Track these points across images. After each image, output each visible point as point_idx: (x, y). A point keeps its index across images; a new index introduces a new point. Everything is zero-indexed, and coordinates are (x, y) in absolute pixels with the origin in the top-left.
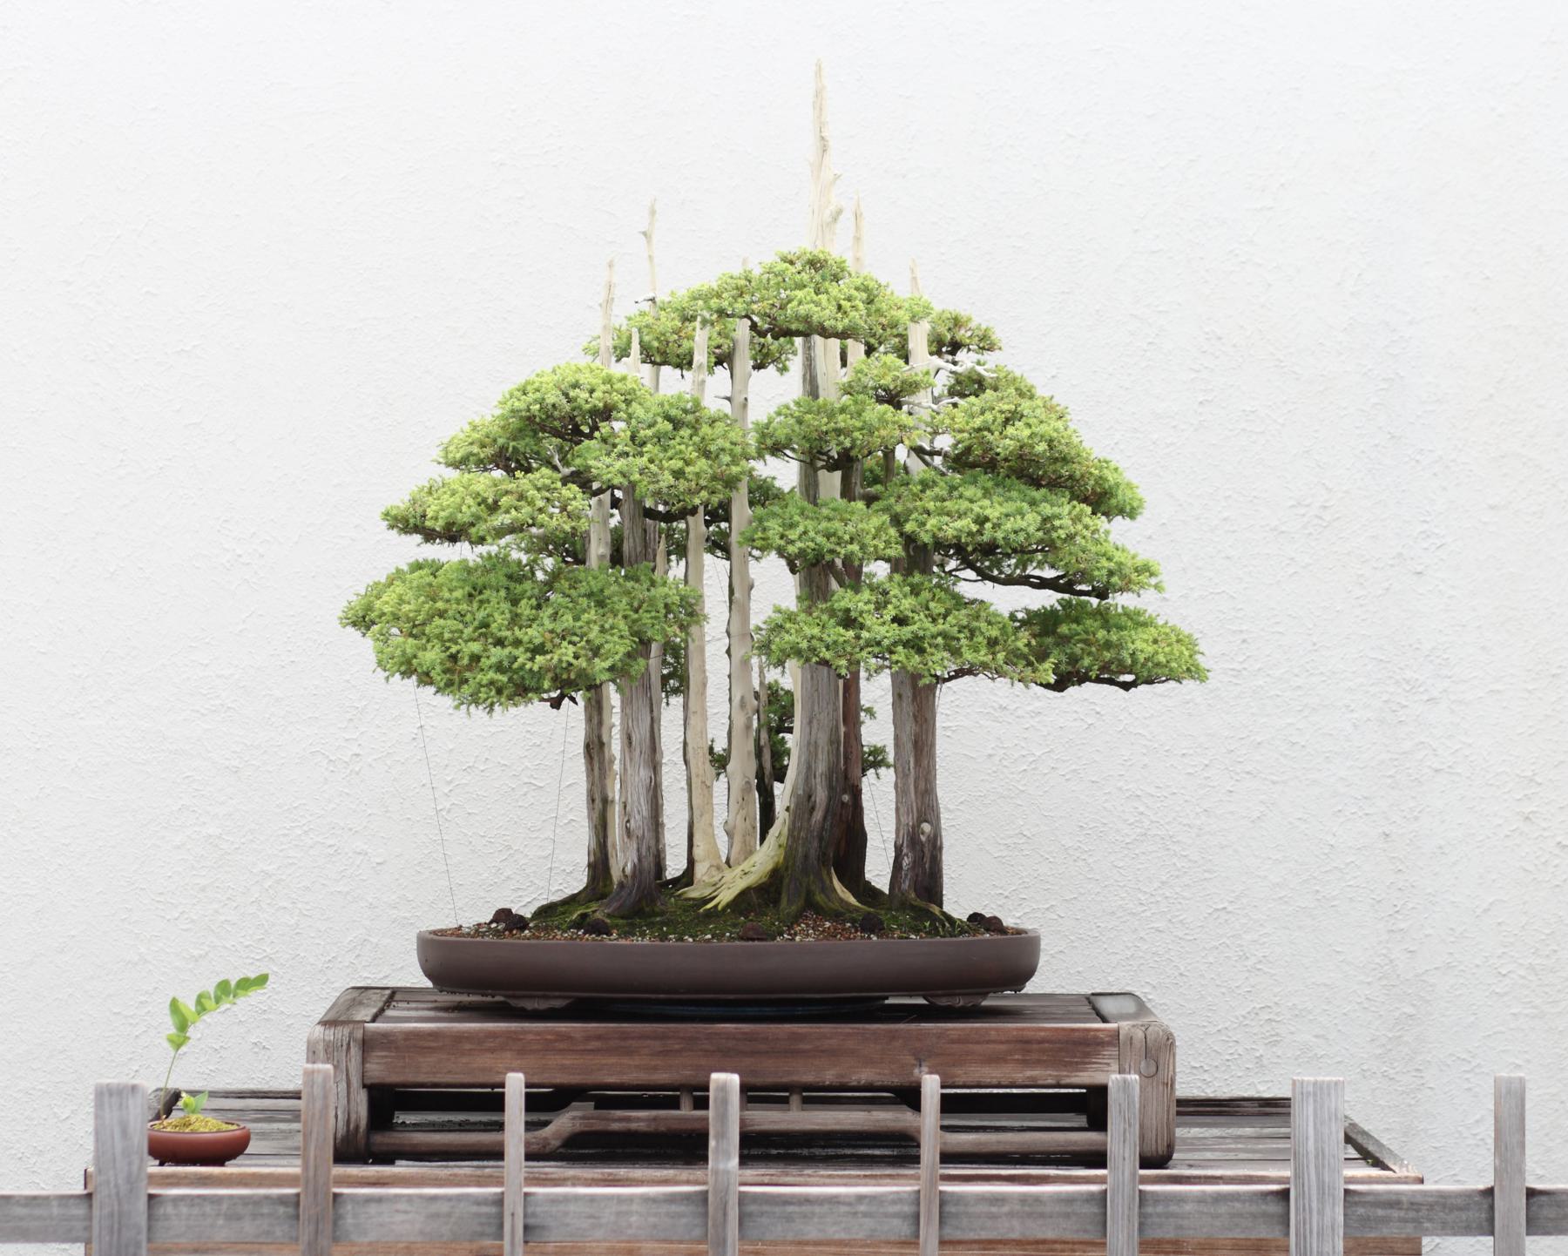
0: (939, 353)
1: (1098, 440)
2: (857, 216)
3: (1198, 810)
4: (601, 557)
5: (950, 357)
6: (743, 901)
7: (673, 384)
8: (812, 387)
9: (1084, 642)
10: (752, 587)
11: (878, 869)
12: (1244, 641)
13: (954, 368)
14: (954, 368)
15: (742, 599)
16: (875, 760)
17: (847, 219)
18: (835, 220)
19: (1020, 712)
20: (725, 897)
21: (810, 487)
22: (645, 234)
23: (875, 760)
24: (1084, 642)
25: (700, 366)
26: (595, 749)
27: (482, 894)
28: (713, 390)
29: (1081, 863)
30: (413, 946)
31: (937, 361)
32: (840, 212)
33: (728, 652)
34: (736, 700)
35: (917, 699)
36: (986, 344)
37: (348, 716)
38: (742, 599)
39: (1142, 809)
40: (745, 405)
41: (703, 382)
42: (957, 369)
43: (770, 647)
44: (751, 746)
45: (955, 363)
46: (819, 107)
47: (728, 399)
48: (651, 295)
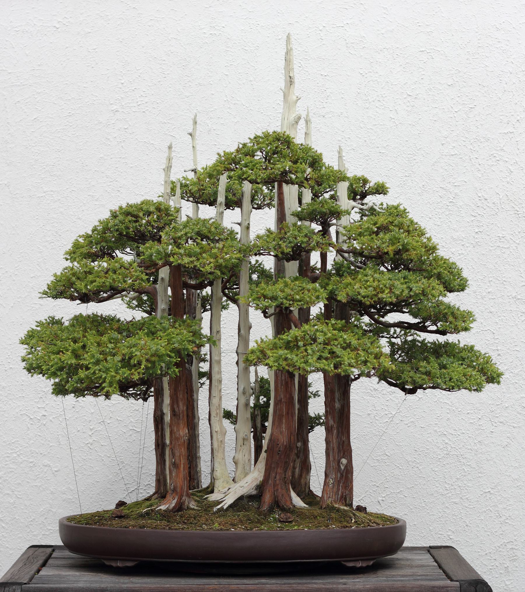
0: (354, 199)
1: (449, 246)
2: (307, 122)
3: (476, 441)
4: (163, 310)
5: (360, 202)
6: (239, 504)
7: (207, 212)
8: (281, 217)
9: (438, 361)
10: (250, 327)
11: (317, 482)
12: (499, 355)
13: (362, 207)
14: (362, 207)
15: (234, 336)
16: (314, 422)
17: (302, 122)
18: (297, 123)
19: (384, 392)
20: (229, 501)
21: (280, 270)
22: (191, 135)
23: (314, 422)
24: (438, 361)
25: (221, 204)
26: (158, 420)
27: (109, 486)
28: (231, 218)
29: (416, 469)
30: (56, 527)
31: (352, 203)
32: (299, 118)
33: (237, 363)
34: (241, 389)
35: (339, 388)
36: (380, 190)
37: (40, 396)
38: (234, 336)
39: (447, 441)
40: (248, 228)
41: (223, 212)
42: (365, 207)
43: (261, 356)
44: (249, 416)
45: (363, 204)
46: (288, 61)
47: (239, 224)
48: (194, 168)
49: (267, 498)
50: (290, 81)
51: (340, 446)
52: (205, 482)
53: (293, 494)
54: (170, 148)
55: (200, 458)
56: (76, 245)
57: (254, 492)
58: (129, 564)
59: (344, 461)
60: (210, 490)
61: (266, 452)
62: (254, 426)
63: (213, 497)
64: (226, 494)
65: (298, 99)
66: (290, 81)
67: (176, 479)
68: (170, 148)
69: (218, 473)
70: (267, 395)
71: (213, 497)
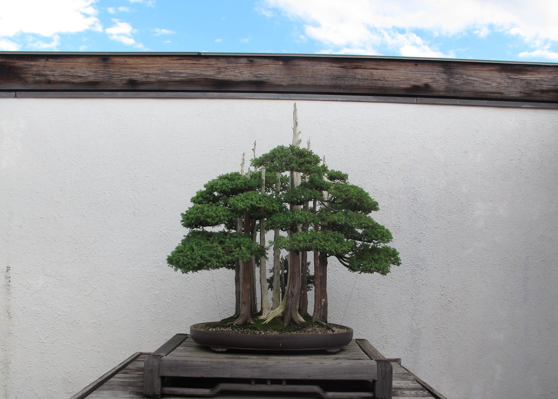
9: (372, 254)
11: (310, 310)
24: (372, 254)
26: (237, 280)
35: (322, 263)
49: (287, 319)
50: (296, 124)
51: (322, 294)
52: (259, 310)
53: (299, 315)
54: (244, 154)
55: (367, 194)
56: (193, 198)
57: (281, 315)
58: (224, 350)
59: (324, 300)
60: (261, 313)
61: (309, 264)
62: (282, 283)
63: (262, 317)
64: (268, 316)
65: (300, 132)
66: (296, 124)
67: (245, 310)
68: (244, 154)
69: (264, 306)
70: (287, 269)
71: (262, 317)
